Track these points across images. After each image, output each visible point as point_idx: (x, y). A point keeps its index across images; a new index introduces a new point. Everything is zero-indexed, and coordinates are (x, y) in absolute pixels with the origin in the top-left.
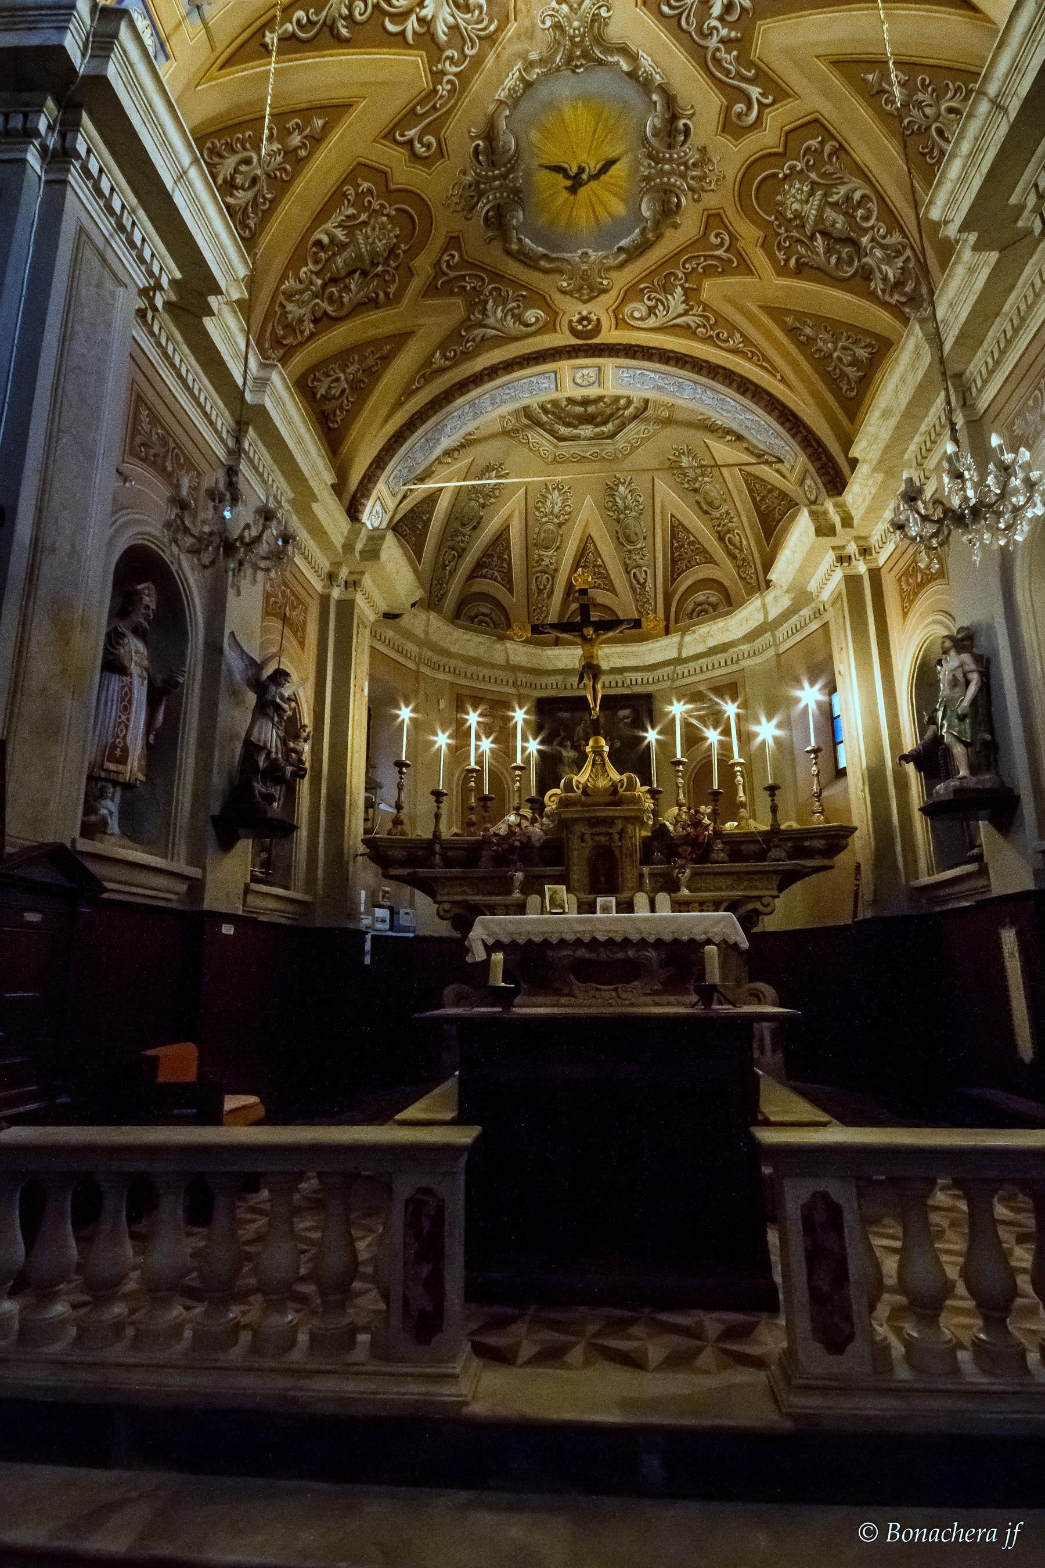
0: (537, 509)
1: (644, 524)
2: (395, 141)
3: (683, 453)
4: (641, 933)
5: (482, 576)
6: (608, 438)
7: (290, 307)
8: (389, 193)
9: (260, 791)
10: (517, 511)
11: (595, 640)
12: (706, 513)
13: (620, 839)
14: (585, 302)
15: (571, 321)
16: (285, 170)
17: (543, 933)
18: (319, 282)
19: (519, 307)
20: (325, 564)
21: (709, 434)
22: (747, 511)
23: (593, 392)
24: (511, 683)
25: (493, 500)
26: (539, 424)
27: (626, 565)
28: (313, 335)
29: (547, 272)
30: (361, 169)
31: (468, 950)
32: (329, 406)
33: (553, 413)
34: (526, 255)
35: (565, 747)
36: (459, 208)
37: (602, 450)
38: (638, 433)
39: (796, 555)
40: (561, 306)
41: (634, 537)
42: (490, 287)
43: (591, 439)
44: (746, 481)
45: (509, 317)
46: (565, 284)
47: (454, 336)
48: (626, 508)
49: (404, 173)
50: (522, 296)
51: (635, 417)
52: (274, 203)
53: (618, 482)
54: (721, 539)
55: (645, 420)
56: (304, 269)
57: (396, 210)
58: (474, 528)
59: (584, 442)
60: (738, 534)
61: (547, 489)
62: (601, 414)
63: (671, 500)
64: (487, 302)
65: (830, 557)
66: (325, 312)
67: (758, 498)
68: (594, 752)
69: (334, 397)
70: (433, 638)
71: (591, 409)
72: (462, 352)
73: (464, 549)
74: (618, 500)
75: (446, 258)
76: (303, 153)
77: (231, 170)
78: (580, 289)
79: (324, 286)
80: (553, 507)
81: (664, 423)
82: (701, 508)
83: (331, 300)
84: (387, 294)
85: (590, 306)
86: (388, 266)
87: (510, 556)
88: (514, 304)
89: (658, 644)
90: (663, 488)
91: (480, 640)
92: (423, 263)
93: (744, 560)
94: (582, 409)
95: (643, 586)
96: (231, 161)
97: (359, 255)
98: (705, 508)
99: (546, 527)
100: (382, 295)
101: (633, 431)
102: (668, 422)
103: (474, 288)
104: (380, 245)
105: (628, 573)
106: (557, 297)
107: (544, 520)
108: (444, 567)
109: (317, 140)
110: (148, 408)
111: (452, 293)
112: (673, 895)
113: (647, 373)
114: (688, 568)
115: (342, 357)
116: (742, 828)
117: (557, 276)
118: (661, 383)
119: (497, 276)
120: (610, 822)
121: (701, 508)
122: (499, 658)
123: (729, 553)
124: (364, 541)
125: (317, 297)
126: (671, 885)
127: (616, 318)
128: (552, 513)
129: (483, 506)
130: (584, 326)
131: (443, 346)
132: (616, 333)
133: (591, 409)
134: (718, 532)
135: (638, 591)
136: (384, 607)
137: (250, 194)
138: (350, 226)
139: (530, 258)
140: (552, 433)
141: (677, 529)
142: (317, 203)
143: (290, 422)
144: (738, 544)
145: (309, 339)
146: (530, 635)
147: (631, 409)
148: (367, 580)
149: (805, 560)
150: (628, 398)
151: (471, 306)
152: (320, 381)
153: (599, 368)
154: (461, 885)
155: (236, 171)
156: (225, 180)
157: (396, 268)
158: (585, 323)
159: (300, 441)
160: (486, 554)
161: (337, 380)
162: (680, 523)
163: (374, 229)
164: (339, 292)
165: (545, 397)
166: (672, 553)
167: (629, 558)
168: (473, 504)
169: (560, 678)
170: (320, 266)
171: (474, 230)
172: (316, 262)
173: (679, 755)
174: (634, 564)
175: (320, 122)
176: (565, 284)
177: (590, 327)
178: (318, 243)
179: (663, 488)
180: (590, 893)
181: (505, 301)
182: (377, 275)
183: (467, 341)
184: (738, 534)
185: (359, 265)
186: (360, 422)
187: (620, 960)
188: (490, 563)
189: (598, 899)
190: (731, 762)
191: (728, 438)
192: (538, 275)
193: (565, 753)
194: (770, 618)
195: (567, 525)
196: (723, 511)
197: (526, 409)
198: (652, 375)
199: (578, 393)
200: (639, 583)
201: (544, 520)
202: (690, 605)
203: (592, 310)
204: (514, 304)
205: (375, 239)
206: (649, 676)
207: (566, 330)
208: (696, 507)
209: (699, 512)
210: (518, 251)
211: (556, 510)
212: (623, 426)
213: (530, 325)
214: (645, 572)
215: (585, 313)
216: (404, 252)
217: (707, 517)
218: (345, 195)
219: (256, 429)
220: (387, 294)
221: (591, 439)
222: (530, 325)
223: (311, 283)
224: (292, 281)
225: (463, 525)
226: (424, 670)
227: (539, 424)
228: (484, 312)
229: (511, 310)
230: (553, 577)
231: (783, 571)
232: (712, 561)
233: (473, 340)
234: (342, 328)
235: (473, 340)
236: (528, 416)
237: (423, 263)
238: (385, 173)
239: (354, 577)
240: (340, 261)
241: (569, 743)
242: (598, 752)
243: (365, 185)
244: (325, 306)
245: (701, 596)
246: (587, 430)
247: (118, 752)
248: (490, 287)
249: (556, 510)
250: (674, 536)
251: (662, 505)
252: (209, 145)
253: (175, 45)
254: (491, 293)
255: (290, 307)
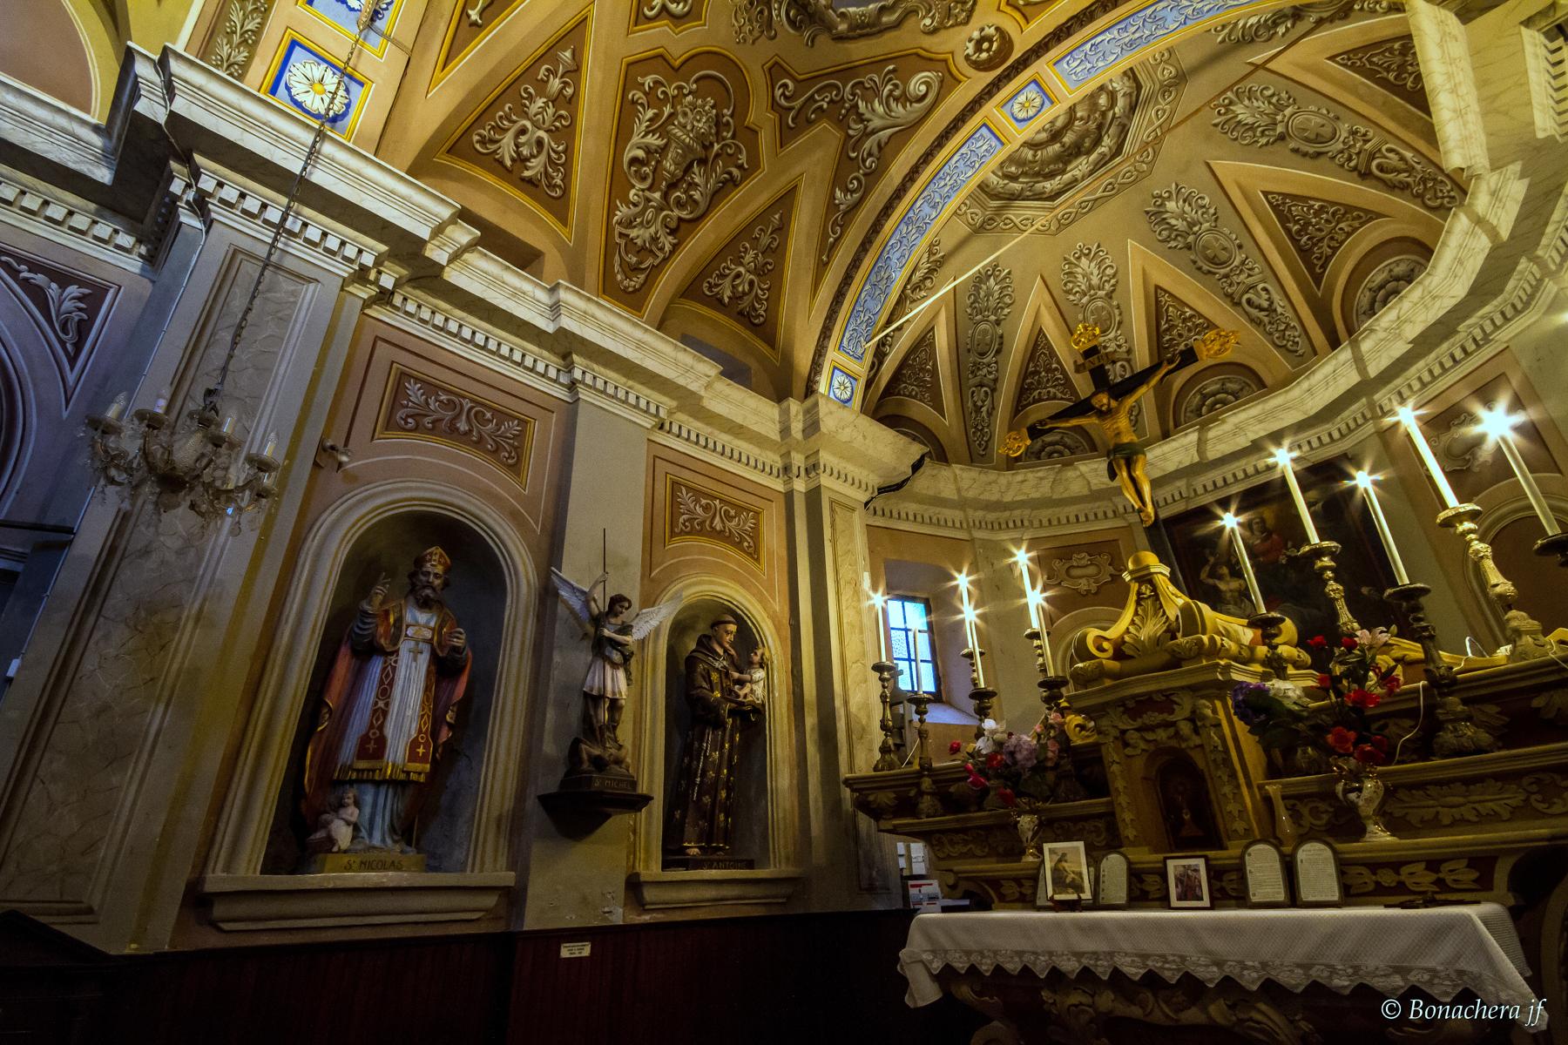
0: (1069, 292)
1: (1229, 227)
2: (650, 19)
3: (1231, 103)
4: (1219, 964)
5: (1035, 401)
6: (1113, 157)
7: (633, 233)
8: (676, 71)
9: (589, 755)
10: (1043, 310)
11: (1117, 410)
12: (1319, 154)
13: (1196, 731)
14: (967, 21)
15: (967, 57)
16: (561, 116)
17: (1020, 954)
18: (657, 195)
19: (896, 86)
20: (774, 459)
21: (1247, 50)
22: (1385, 107)
23: (1055, 113)
24: (1110, 514)
25: (1006, 311)
26: (1014, 197)
27: (1229, 296)
28: (675, 247)
29: (897, 25)
30: (634, 68)
31: (903, 984)
32: (745, 304)
33: (1024, 174)
34: (862, 26)
35: (1220, 578)
36: (756, 33)
37: (1116, 177)
38: (1151, 122)
39: (1463, 90)
40: (947, 48)
41: (1223, 256)
42: (848, 88)
43: (1091, 173)
44: (1352, 67)
45: (893, 105)
46: (928, 21)
47: (844, 167)
48: (1191, 225)
49: (678, 42)
50: (889, 72)
51: (1132, 108)
52: (568, 151)
53: (1161, 200)
54: (1365, 175)
55: (1147, 101)
56: (633, 192)
57: (696, 81)
58: (998, 352)
59: (1086, 182)
60: (1390, 150)
61: (1070, 263)
62: (1086, 134)
63: (1253, 175)
64: (856, 105)
65: (1533, 43)
66: (680, 219)
67: (1391, 77)
68: (1136, 579)
69: (744, 294)
70: (970, 494)
71: (1068, 138)
72: (865, 175)
73: (996, 380)
74: (1173, 222)
75: (778, 92)
76: (569, 91)
77: (512, 146)
78: (949, 14)
79: (665, 196)
80: (1089, 280)
81: (1176, 85)
82: (1305, 155)
83: (680, 204)
84: (740, 167)
85: (976, 21)
86: (724, 139)
87: (1059, 362)
88: (889, 87)
89: (1319, 376)
90: (1228, 168)
91: (1040, 474)
92: (759, 114)
93: (1424, 181)
94: (1057, 147)
95: (1271, 310)
96: (507, 141)
97: (687, 148)
98: (1311, 151)
99: (1092, 306)
100: (736, 172)
101: (1142, 127)
102: (1181, 78)
103: (832, 101)
104: (701, 126)
105: (1237, 304)
106: (928, 42)
107: (1085, 300)
108: (978, 409)
109: (575, 71)
110: (417, 380)
111: (810, 123)
112: (1340, 846)
113: (1099, 39)
114: (1335, 250)
115: (730, 249)
116: (1523, 655)
117: (911, 21)
118: (1127, 37)
119: (848, 72)
120: (1165, 702)
121: (1305, 155)
122: (1077, 488)
123: (1392, 187)
124: (801, 417)
125: (662, 210)
126: (1343, 825)
127: (1017, 8)
128: (1091, 287)
129: (998, 323)
130: (988, 50)
131: (838, 180)
132: (1033, 25)
133: (1068, 138)
134: (1355, 169)
135: (1266, 320)
136: (875, 481)
137: (543, 158)
138: (659, 127)
139: (868, 25)
140: (1039, 196)
141: (1283, 207)
142: (610, 125)
143: (614, 331)
144: (1402, 165)
145: (672, 252)
146: (1029, 442)
147: (1121, 102)
148: (825, 457)
149: (1482, 83)
150: (1102, 88)
151: (841, 123)
152: (717, 285)
153: (1035, 81)
154: (966, 843)
155: (517, 146)
156: (513, 160)
157: (733, 137)
158: (986, 45)
159: (639, 345)
160: (1025, 374)
161: (738, 275)
162: (1285, 196)
163: (685, 114)
164: (685, 192)
165: (993, 162)
166: (1295, 241)
167: (1230, 285)
168: (983, 326)
169: (1181, 484)
170: (649, 181)
171: (789, 43)
172: (643, 179)
173: (1314, 538)
174: (1242, 287)
175: (568, 54)
176: (928, 21)
177: (995, 45)
178: (634, 161)
179: (1228, 168)
180: (1156, 851)
181: (876, 92)
182: (717, 155)
183: (864, 161)
184: (1390, 150)
185: (691, 157)
186: (785, 301)
187: (1195, 1028)
188: (1039, 382)
189: (1171, 864)
190: (1442, 515)
191: (1281, 30)
192: (888, 36)
193: (1222, 586)
194: (1505, 234)
195: (1119, 289)
196: (1344, 134)
197: (983, 187)
198: (1107, 36)
199: (1029, 132)
200: (1262, 310)
201: (1085, 300)
202: (1363, 298)
203: (980, 25)
204: (889, 87)
205: (693, 123)
206: (1334, 427)
207: (970, 71)
208: (1297, 158)
209: (1307, 161)
210: (852, 28)
211: (1095, 281)
212: (1124, 130)
213: (925, 96)
214: (1264, 289)
215: (976, 35)
216: (732, 116)
217: (1323, 160)
218: (634, 102)
219: (580, 354)
220: (740, 167)
221: (1091, 173)
222: (925, 96)
223: (648, 200)
224: (624, 209)
225: (982, 354)
226: (978, 534)
227: (1014, 197)
228: (861, 118)
229: (890, 94)
230: (1128, 361)
231: (1461, 135)
232: (1370, 215)
233: (870, 155)
234: (708, 224)
235: (870, 155)
236: (996, 196)
237: (759, 114)
238: (661, 56)
239: (812, 461)
240: (668, 164)
241: (1225, 570)
242: (1146, 578)
243: (648, 81)
244: (676, 213)
245: (1377, 276)
246: (1080, 166)
247: (372, 746)
248: (848, 88)
249: (1095, 281)
250: (1284, 219)
251: (1240, 187)
252: (476, 138)
253: (363, 69)
254: (854, 95)
255: (633, 233)
